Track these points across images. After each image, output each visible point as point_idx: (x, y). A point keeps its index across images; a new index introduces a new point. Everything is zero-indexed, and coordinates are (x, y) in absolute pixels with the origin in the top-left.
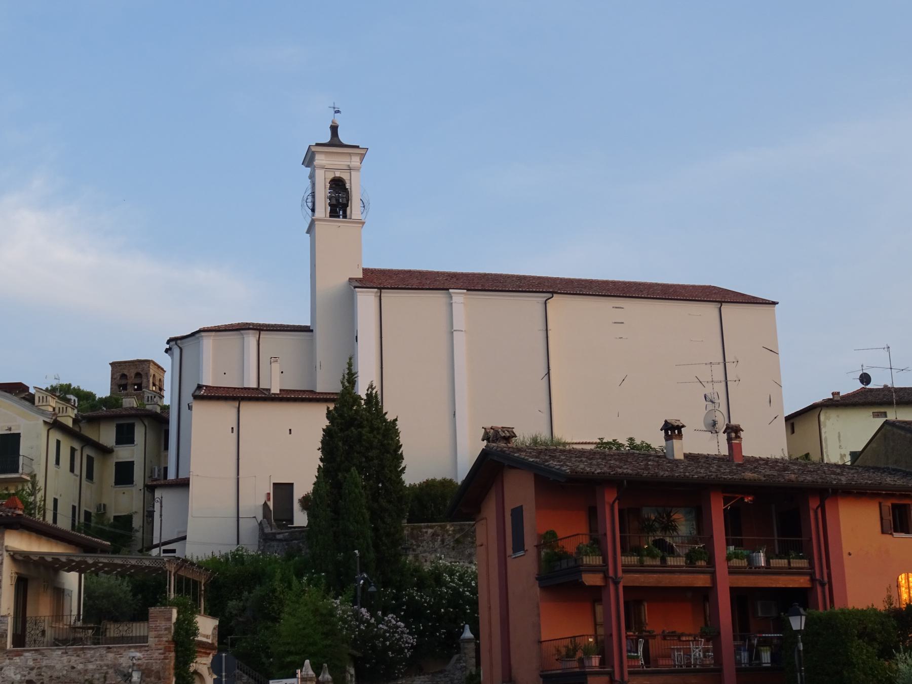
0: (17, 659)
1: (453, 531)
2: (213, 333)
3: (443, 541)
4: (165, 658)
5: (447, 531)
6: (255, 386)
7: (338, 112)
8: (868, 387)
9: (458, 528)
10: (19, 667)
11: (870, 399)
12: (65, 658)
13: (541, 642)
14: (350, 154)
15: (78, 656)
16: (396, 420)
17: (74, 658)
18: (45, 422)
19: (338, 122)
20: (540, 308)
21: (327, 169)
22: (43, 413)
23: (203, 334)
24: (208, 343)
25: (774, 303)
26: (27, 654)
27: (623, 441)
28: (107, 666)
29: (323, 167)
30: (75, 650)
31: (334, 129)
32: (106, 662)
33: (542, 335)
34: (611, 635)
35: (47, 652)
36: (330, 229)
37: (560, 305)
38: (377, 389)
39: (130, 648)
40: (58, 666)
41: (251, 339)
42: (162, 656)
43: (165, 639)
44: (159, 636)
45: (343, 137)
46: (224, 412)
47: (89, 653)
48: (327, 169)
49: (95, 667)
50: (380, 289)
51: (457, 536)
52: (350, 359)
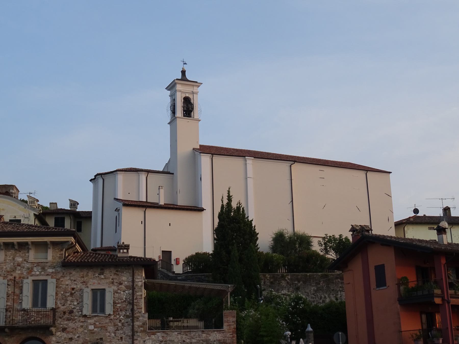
0: (153, 337)
1: (270, 277)
2: (123, 172)
3: (265, 282)
4: (233, 337)
5: (267, 277)
6: (145, 201)
7: (186, 64)
8: (417, 215)
9: (272, 276)
10: (155, 340)
11: (418, 221)
12: (179, 336)
13: (401, 332)
14: (193, 85)
15: (187, 335)
16: (252, 220)
17: (184, 336)
18: (34, 214)
19: (185, 69)
20: (288, 168)
21: (182, 92)
22: (33, 209)
23: (118, 172)
24: (120, 177)
25: (390, 173)
26: (158, 334)
27: (337, 236)
28: (203, 340)
29: (180, 91)
30: (185, 332)
31: (183, 72)
32: (202, 338)
33: (289, 182)
34: (448, 328)
35: (169, 333)
36: (182, 122)
37: (296, 167)
38: (243, 205)
39: (214, 331)
40: (176, 340)
41: (143, 176)
42: (232, 336)
43: (233, 327)
44: (229, 325)
45: (188, 76)
46: (138, 213)
47: (193, 334)
48: (182, 92)
49: (196, 341)
50: (213, 154)
51: (272, 280)
52: (229, 189)
